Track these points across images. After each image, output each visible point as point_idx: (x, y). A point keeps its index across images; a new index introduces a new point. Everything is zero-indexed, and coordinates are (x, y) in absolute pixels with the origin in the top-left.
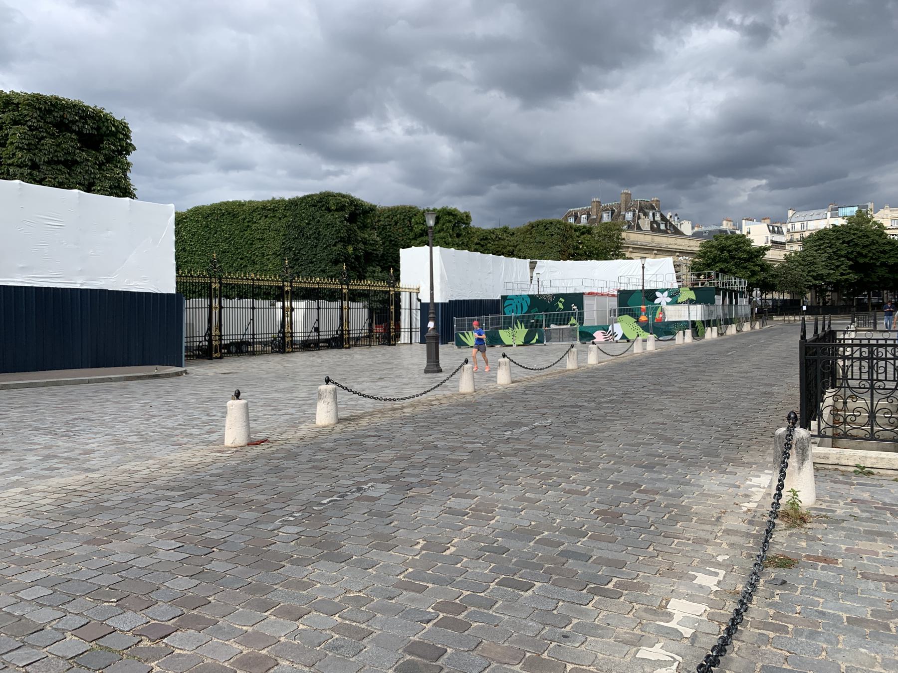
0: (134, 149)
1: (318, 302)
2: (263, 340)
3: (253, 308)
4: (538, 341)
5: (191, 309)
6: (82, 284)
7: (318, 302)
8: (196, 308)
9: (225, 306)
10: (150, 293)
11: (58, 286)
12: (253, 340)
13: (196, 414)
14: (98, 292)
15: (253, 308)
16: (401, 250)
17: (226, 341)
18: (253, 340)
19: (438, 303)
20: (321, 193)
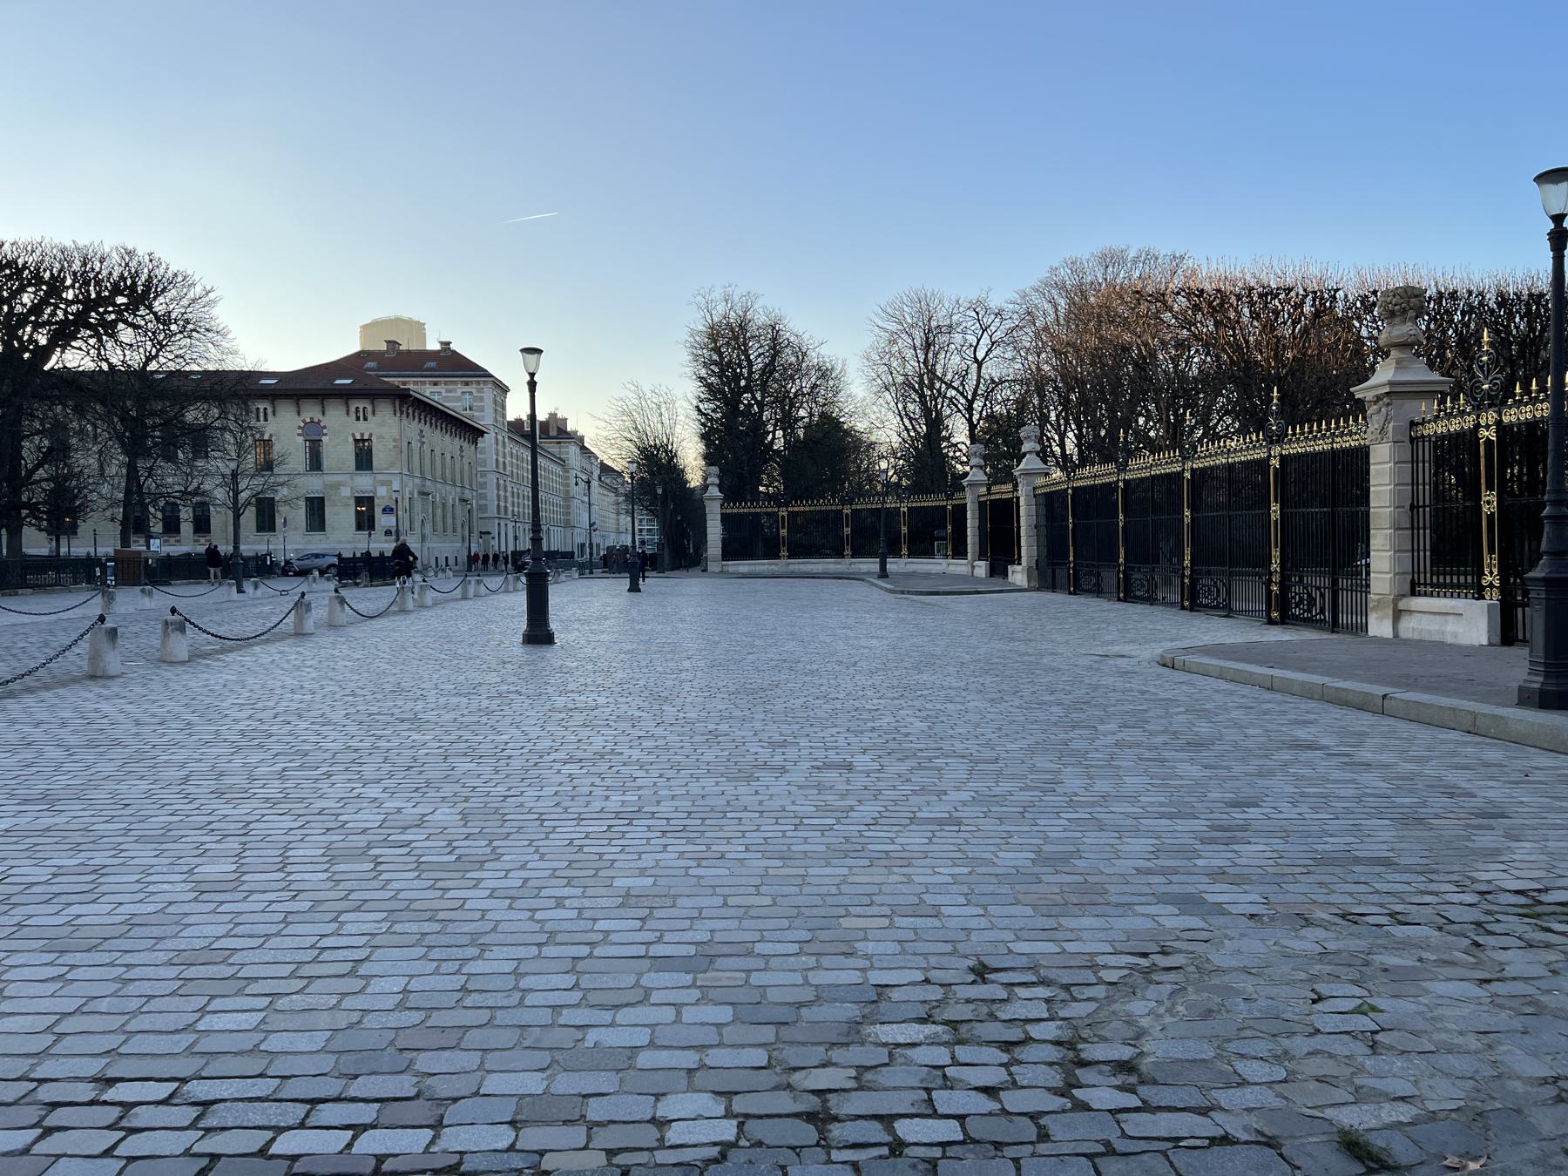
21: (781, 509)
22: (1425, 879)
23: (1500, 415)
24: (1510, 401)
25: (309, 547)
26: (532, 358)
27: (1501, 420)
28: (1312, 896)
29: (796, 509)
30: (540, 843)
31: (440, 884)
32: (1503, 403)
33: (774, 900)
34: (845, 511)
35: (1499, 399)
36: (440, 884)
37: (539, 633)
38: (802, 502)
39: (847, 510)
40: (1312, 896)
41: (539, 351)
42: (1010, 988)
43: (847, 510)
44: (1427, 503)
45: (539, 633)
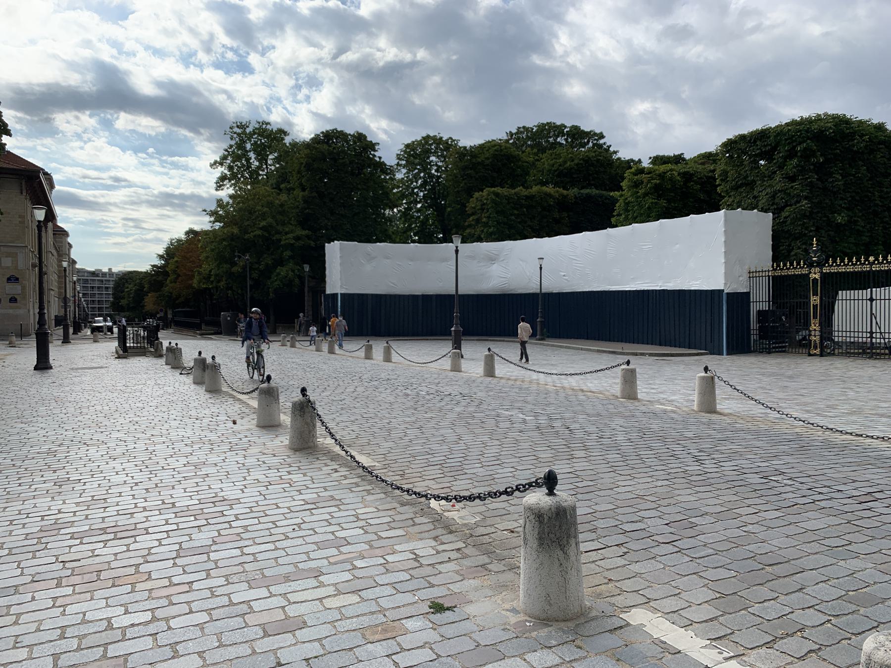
0: (683, 154)
1: (871, 291)
2: (856, 339)
3: (871, 300)
4: (75, 333)
5: (761, 303)
6: (661, 286)
7: (871, 291)
8: (756, 302)
9: (878, 298)
10: (367, 295)
11: (627, 289)
12: (871, 340)
13: (605, 385)
14: (658, 292)
15: (871, 300)
16: (326, 244)
17: (840, 338)
18: (871, 340)
19: (335, 296)
20: (70, 246)
21: (813, 270)
22: (833, 487)
23: (822, 270)
24: (827, 265)
25: (52, 142)
26: (541, 260)
27: (822, 271)
28: (576, 484)
29: (834, 270)
30: (68, 600)
31: (43, 540)
32: (824, 265)
33: (227, 580)
34: (812, 276)
35: (820, 264)
36: (43, 540)
37: (43, 364)
38: (858, 260)
39: (815, 275)
40: (576, 484)
41: (543, 259)
42: (317, 578)
43: (815, 275)
44: (752, 303)
45: (43, 364)
